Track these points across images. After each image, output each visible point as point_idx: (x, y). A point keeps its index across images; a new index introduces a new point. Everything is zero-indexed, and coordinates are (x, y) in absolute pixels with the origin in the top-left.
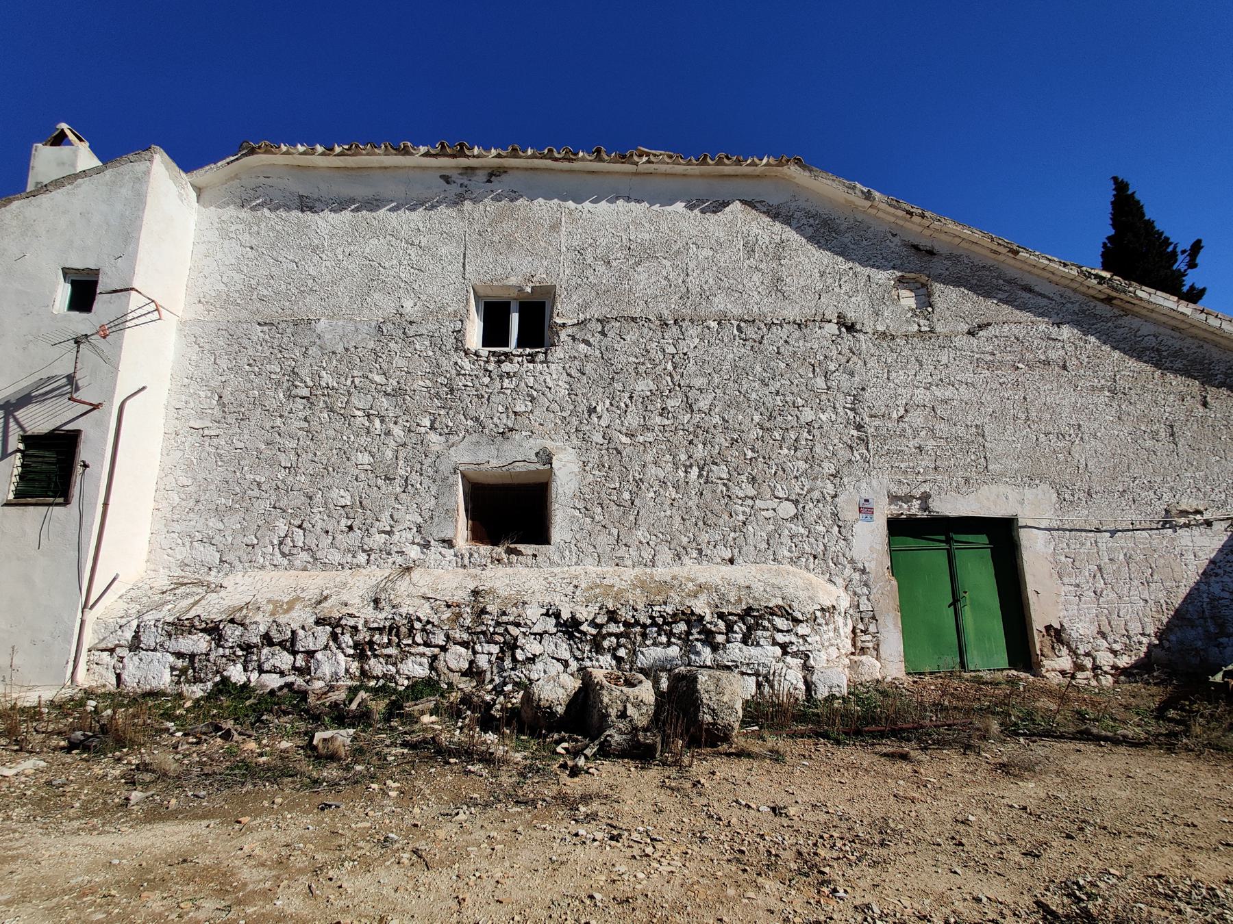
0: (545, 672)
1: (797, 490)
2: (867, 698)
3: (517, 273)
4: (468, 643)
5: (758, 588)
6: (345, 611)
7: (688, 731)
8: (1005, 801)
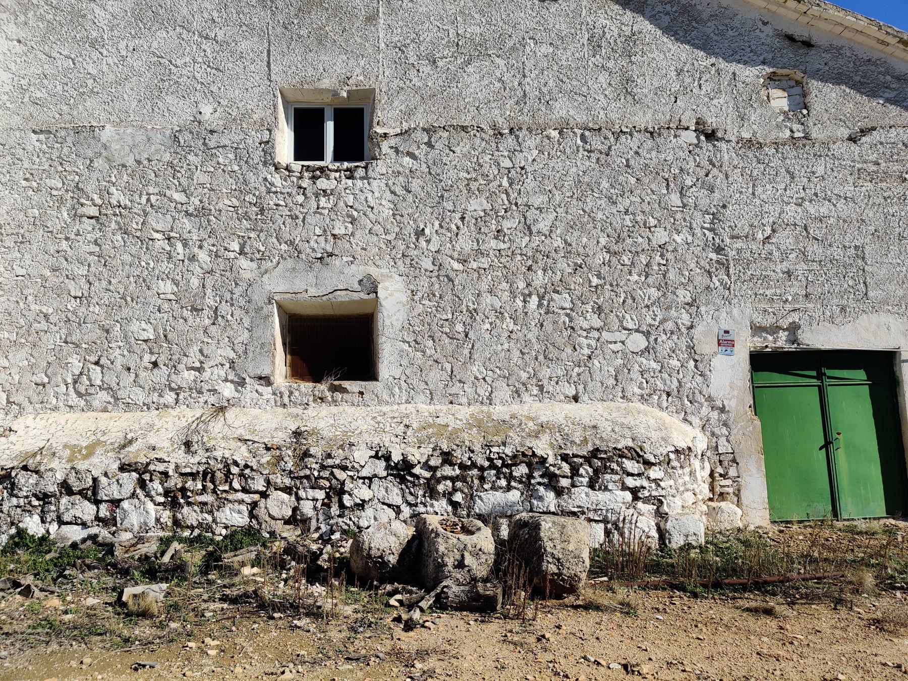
0: (375, 519)
1: (649, 320)
2: (727, 548)
4: (290, 488)
5: (605, 428)
6: (153, 455)
7: (531, 581)
8: (879, 659)
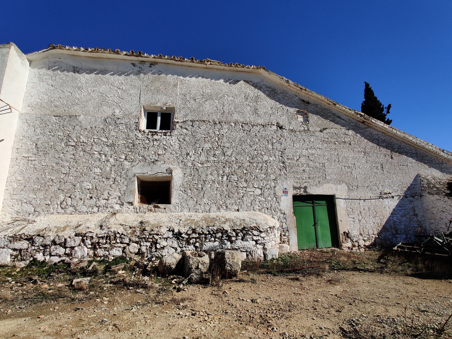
3: (160, 102)
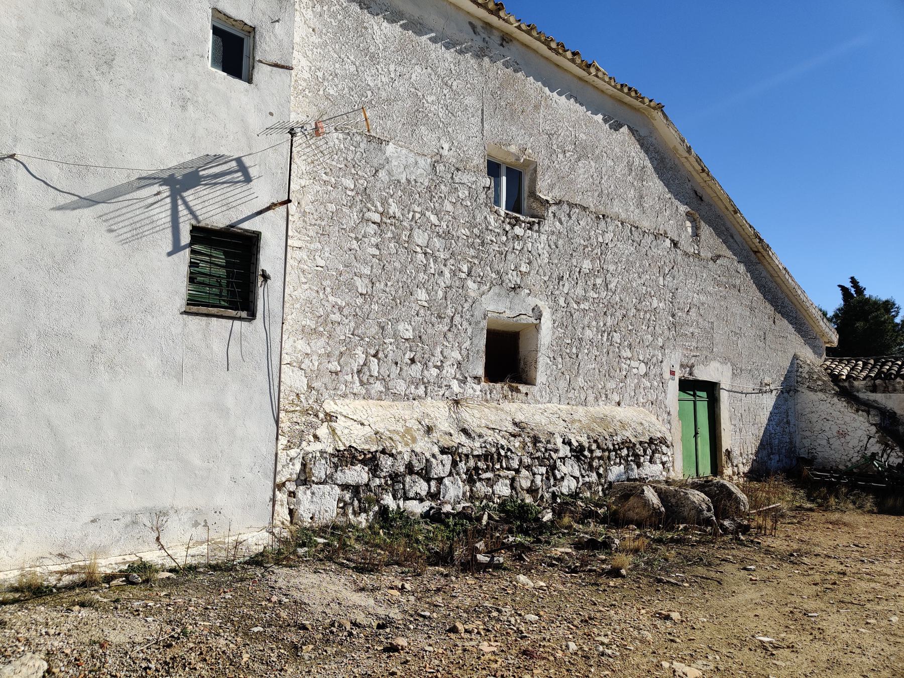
3: (517, 144)
